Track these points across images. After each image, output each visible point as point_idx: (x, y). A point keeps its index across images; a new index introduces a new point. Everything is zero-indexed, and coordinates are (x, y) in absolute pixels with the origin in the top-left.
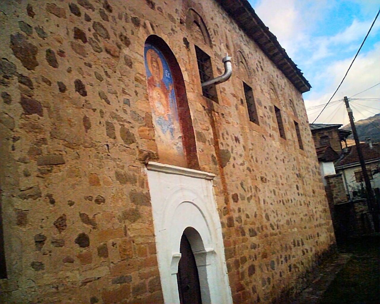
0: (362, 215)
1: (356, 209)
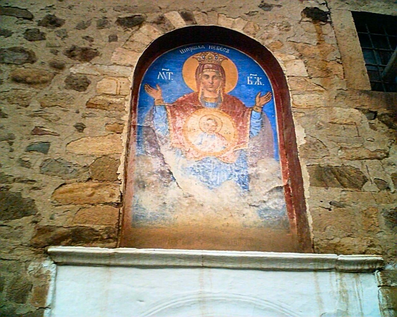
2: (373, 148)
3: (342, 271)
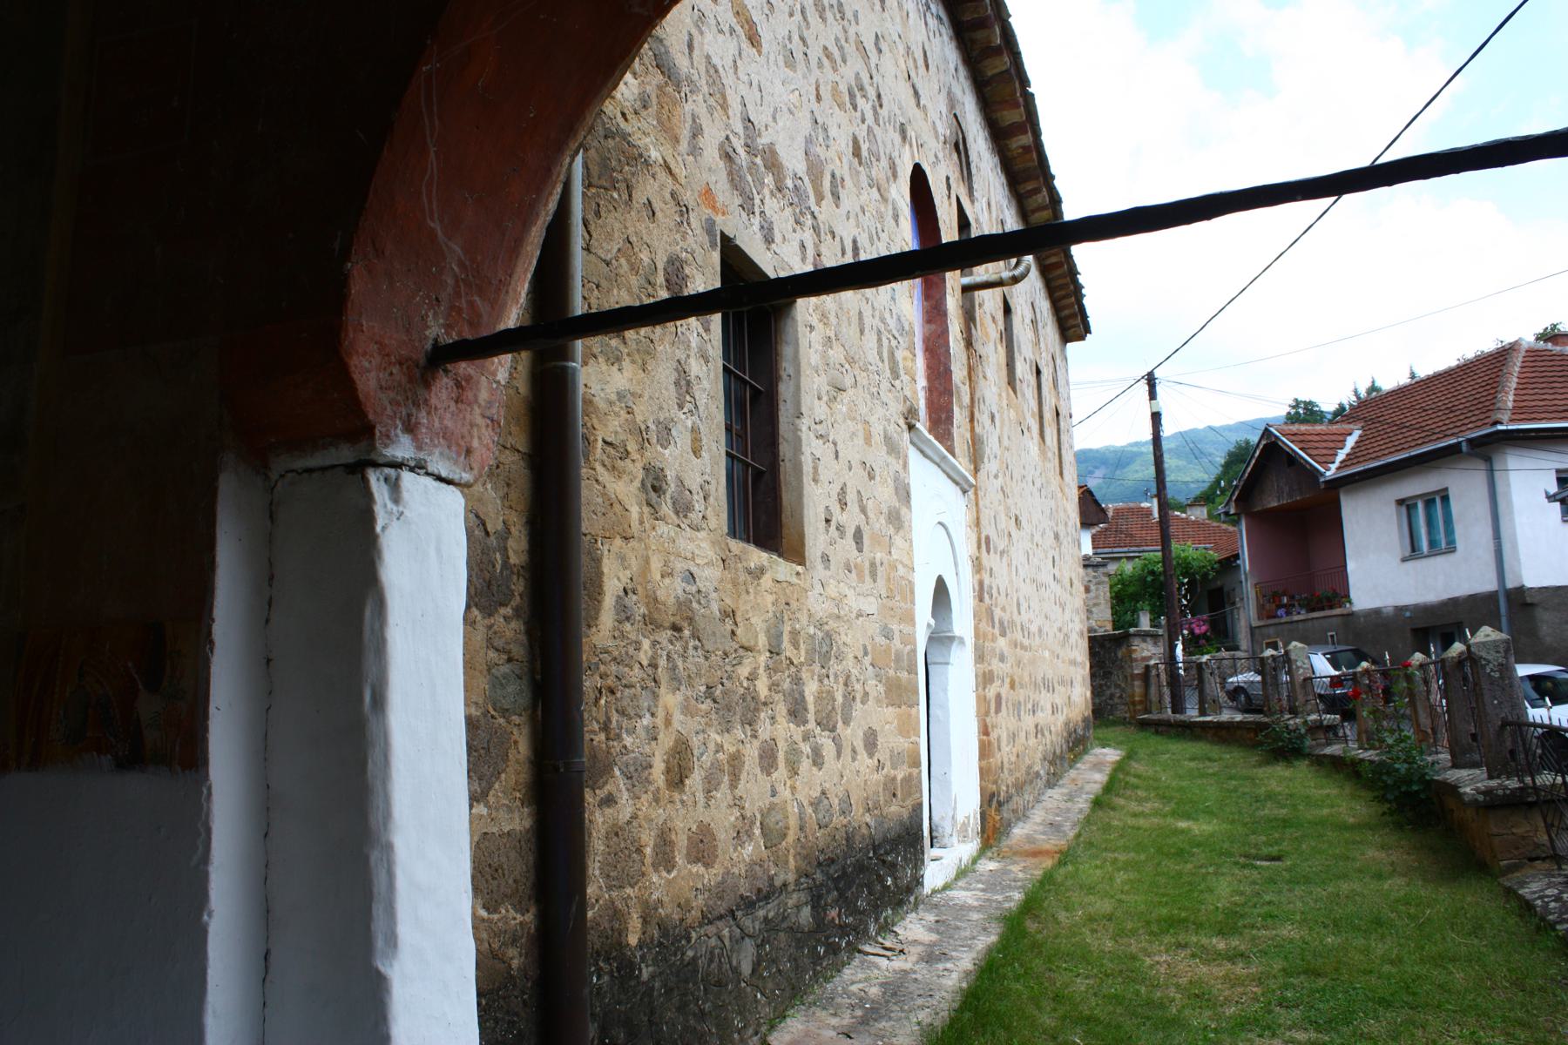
0: (1147, 668)
1: (1135, 650)
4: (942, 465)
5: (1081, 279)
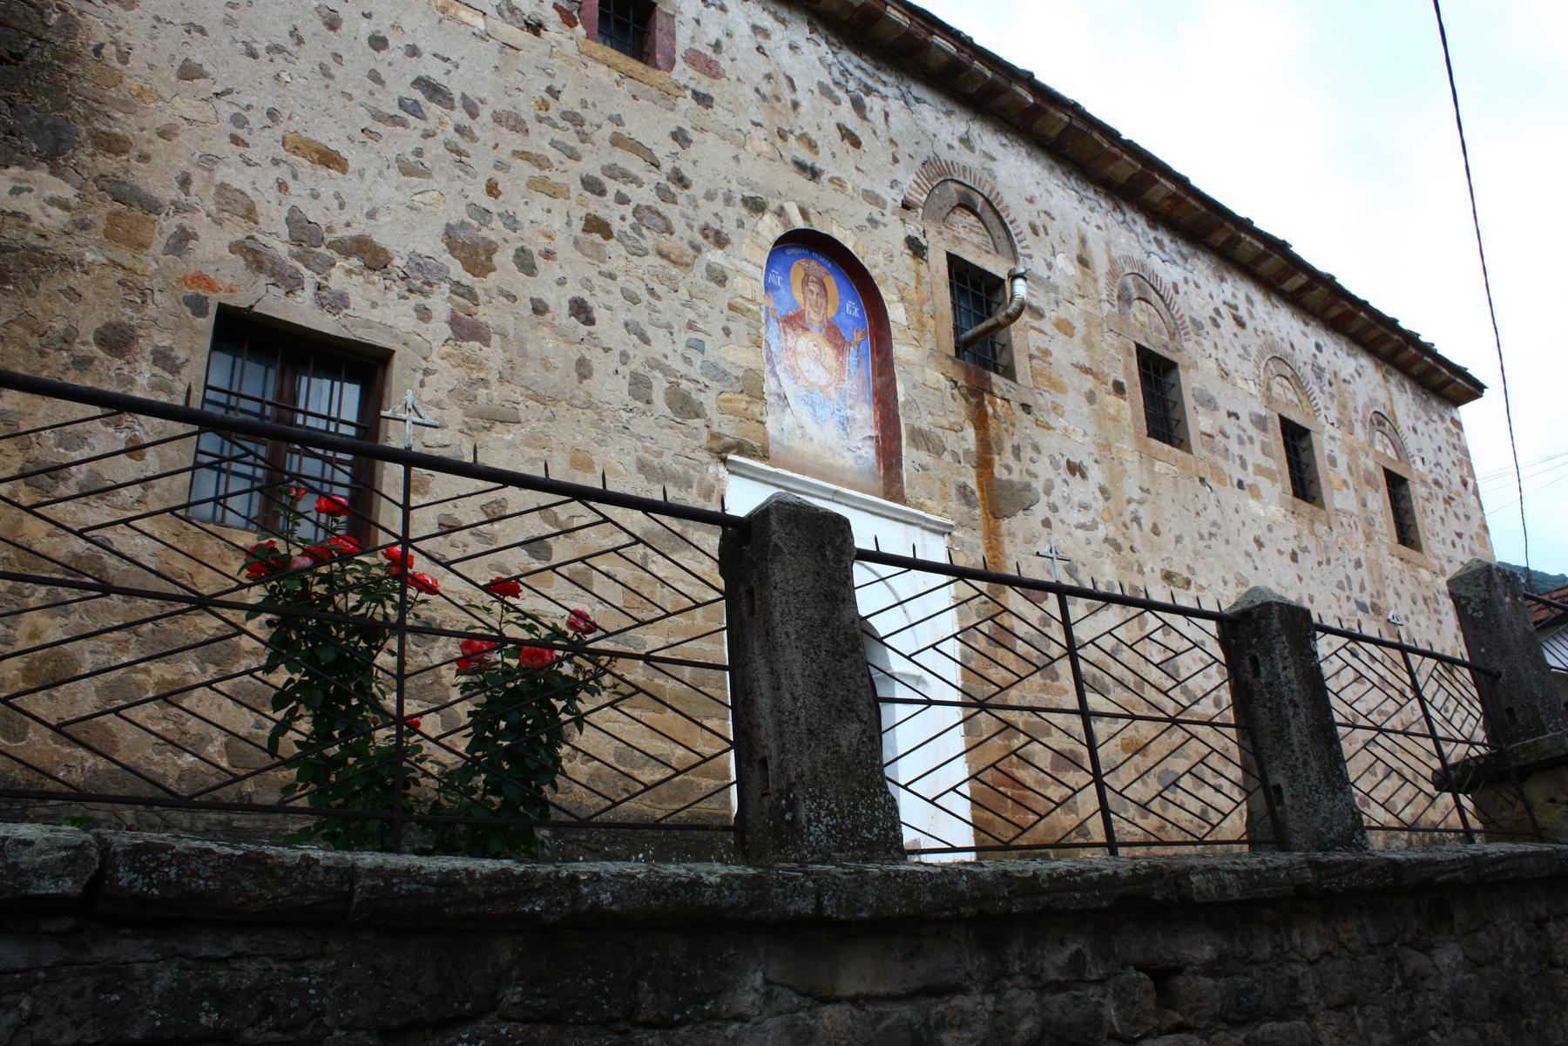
2: (952, 420)
3: (924, 528)
4: (836, 498)
5: (1405, 324)
